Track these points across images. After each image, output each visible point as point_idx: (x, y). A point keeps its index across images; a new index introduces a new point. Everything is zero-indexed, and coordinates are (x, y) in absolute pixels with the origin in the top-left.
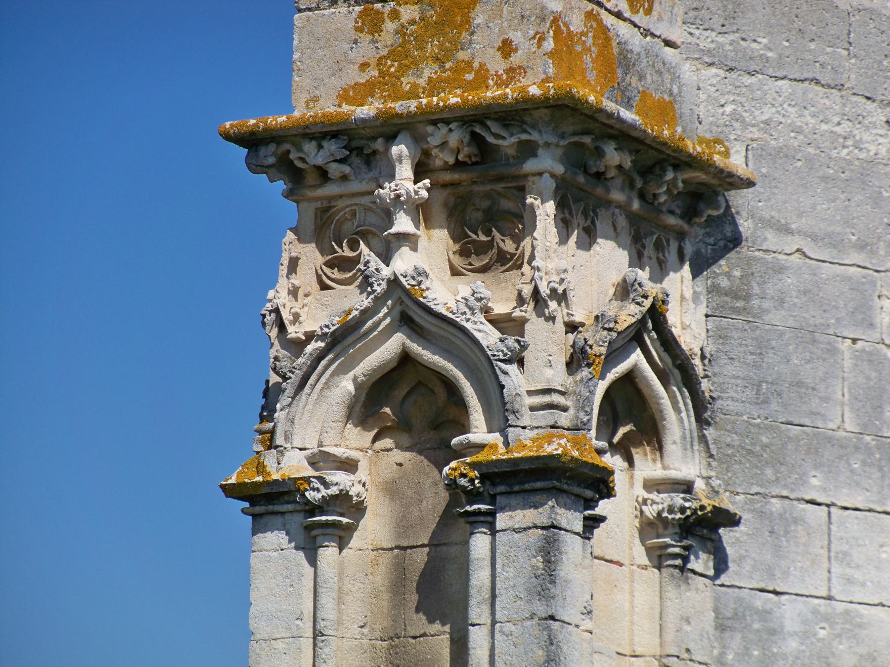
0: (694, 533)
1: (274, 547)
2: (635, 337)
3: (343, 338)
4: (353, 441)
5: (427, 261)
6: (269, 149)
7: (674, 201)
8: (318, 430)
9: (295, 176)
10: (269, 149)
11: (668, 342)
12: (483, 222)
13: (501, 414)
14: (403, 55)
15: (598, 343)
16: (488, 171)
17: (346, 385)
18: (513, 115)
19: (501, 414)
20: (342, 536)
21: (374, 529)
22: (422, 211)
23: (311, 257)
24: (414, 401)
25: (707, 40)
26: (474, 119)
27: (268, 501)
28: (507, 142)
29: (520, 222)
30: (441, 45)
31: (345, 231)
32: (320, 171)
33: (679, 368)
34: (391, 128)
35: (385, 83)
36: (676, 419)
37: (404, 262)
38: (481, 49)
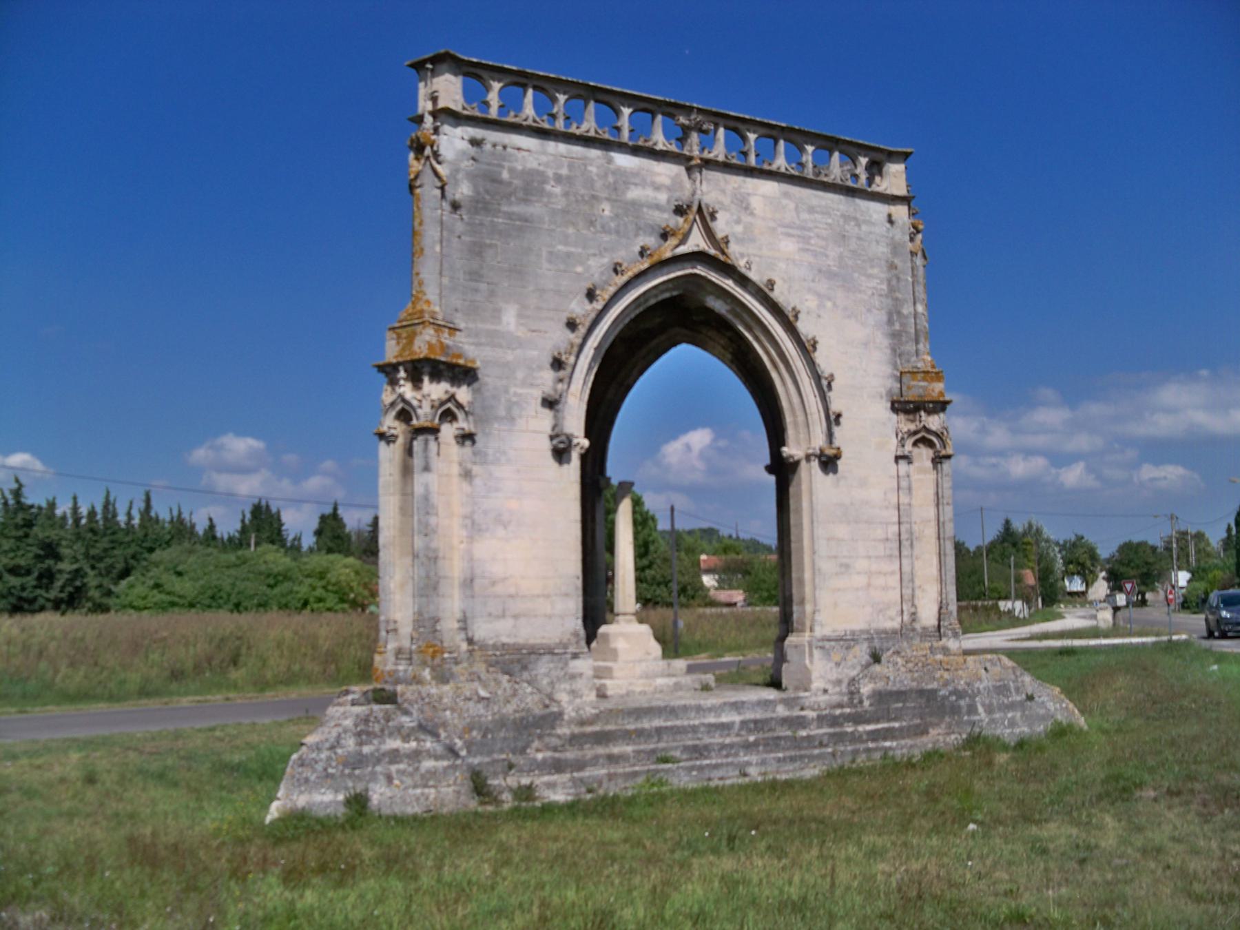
0: (466, 438)
1: (383, 444)
2: (449, 400)
3: (393, 404)
4: (396, 424)
5: (407, 390)
6: (382, 368)
7: (464, 374)
8: (390, 423)
9: (387, 374)
10: (382, 368)
11: (456, 401)
12: (416, 382)
13: (418, 418)
14: (403, 349)
15: (437, 404)
16: (419, 370)
17: (394, 413)
18: (419, 361)
19: (418, 418)
20: (394, 442)
21: (400, 440)
22: (405, 379)
23: (389, 388)
24: (405, 415)
25: (471, 340)
26: (413, 361)
27: (382, 436)
28: (419, 366)
29: (421, 381)
30: (841, 257)
31: (394, 382)
32: (389, 371)
33: (460, 406)
34: (399, 364)
35: (401, 355)
36: (460, 415)
37: (402, 390)
38: (416, 348)
